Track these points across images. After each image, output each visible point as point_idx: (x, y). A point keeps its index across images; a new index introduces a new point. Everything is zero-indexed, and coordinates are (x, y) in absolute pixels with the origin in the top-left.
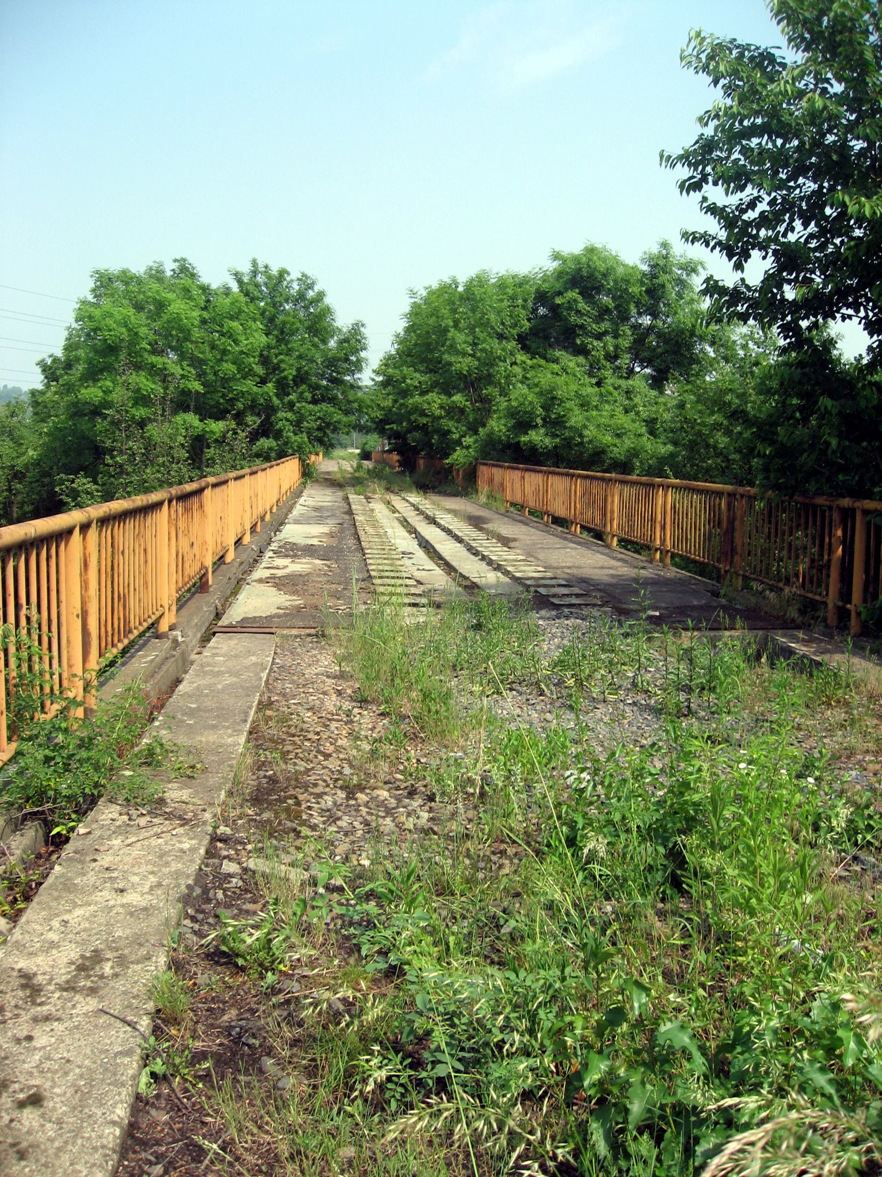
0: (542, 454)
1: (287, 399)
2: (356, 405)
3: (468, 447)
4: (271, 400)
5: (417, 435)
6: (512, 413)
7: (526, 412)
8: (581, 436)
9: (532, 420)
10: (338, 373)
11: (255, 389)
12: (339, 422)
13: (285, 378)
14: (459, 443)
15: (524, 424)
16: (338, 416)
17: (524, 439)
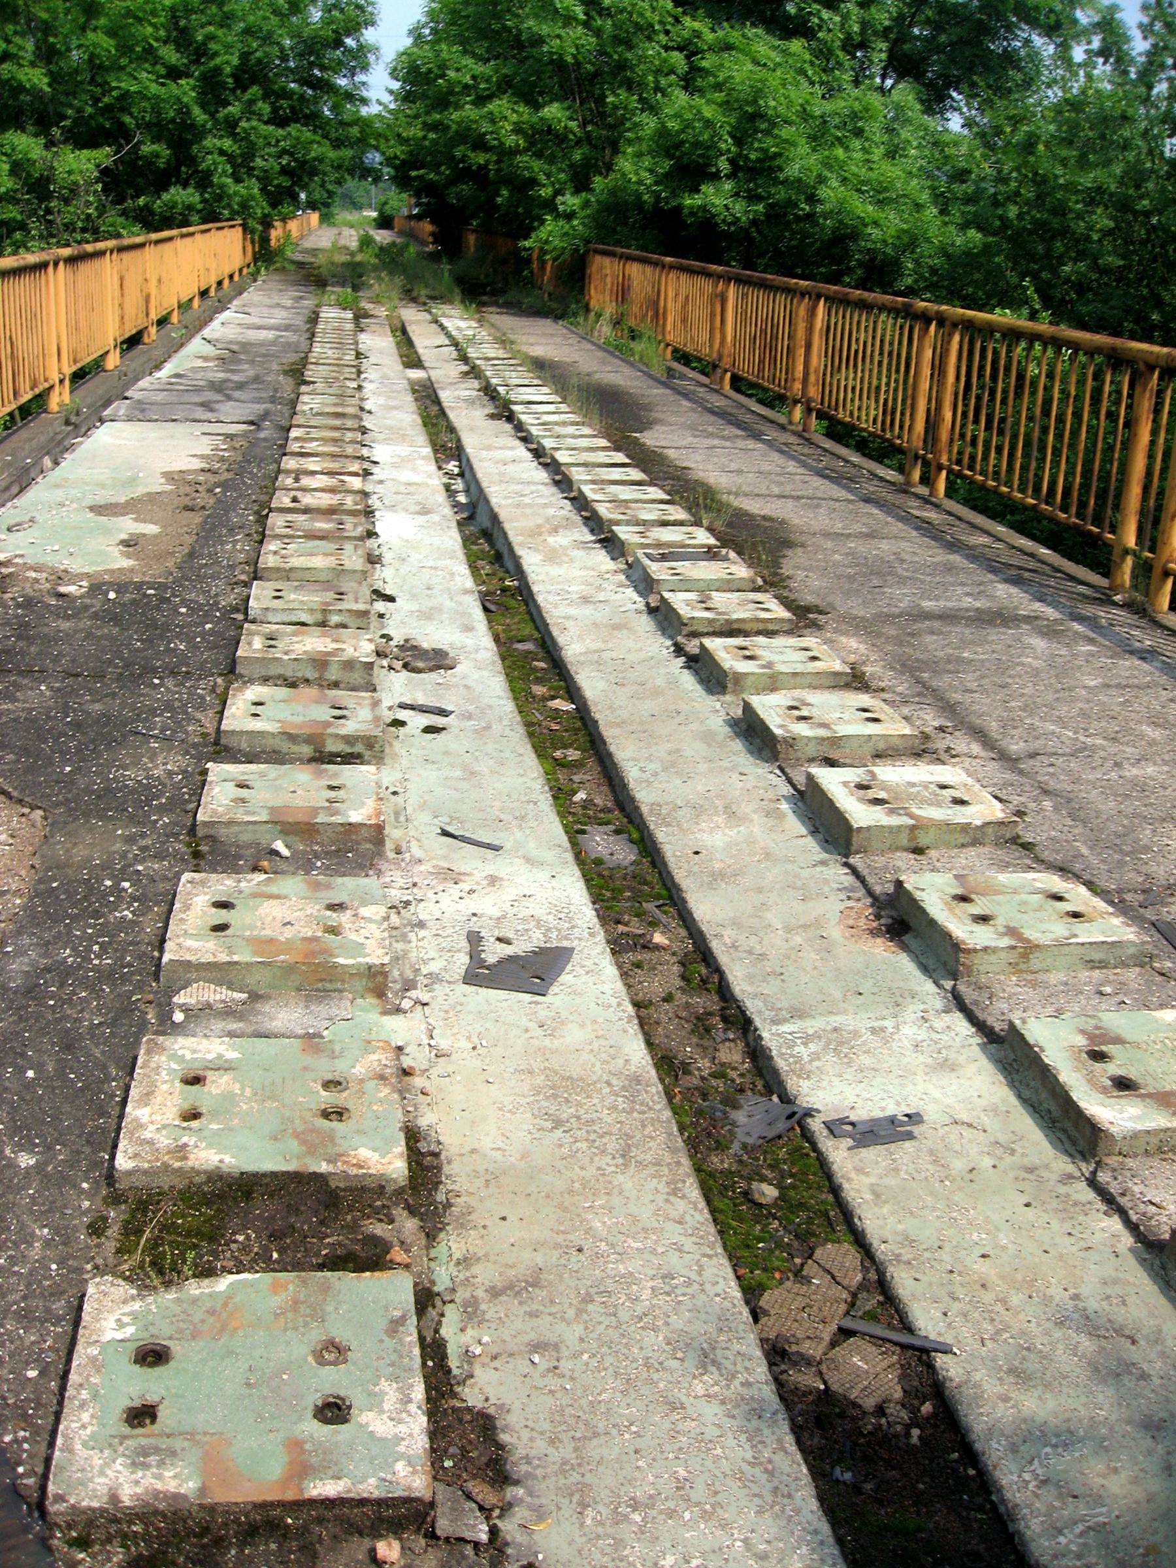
0: (727, 235)
1: (223, 113)
2: (355, 131)
3: (569, 216)
4: (189, 113)
5: (465, 188)
6: (666, 144)
7: (697, 144)
8: (812, 199)
9: (709, 161)
10: (323, 68)
11: (154, 88)
12: (320, 160)
13: (217, 70)
14: (549, 205)
15: (691, 170)
16: (320, 149)
17: (690, 201)
